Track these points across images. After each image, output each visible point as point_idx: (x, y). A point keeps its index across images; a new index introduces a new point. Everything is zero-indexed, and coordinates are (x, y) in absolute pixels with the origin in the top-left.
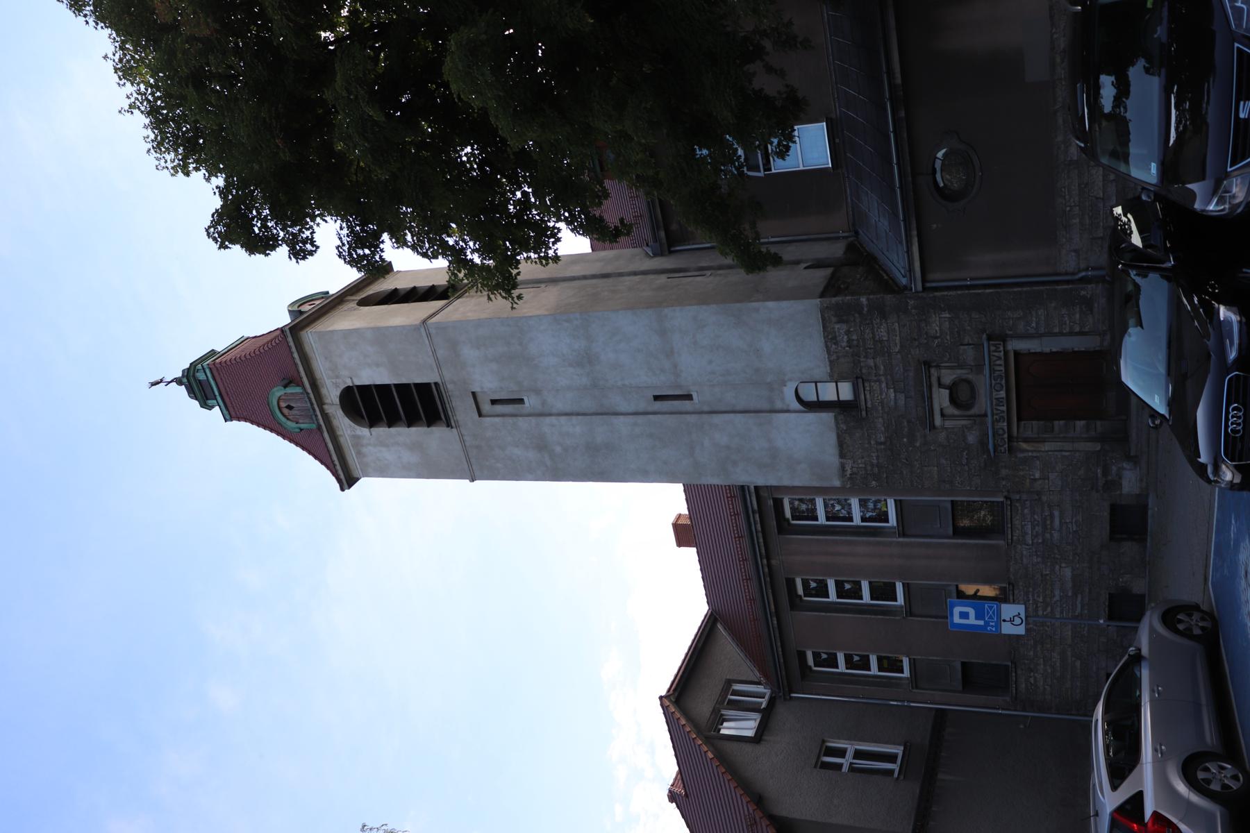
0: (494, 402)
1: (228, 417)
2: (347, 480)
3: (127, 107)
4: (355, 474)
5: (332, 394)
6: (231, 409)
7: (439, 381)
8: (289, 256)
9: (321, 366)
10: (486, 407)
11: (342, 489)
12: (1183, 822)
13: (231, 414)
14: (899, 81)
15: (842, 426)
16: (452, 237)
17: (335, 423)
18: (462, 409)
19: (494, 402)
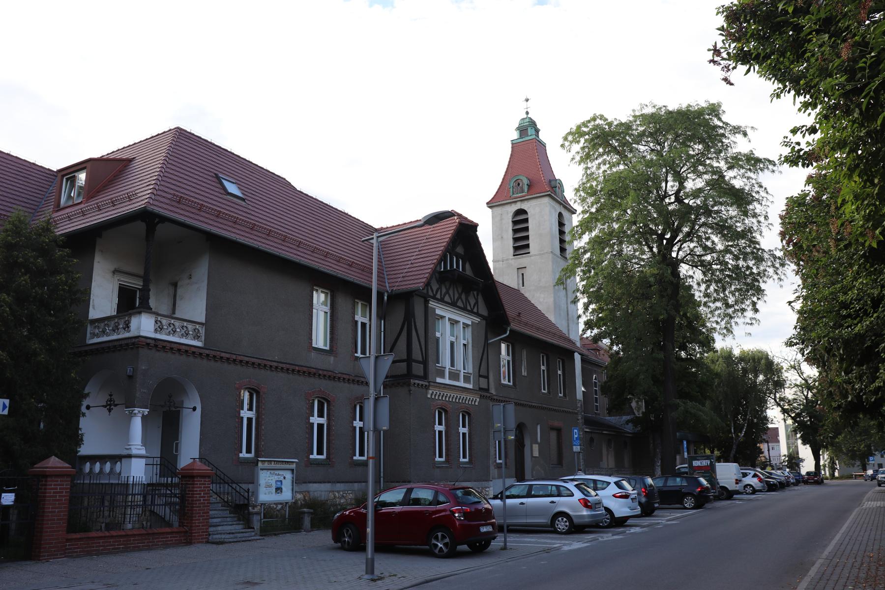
0: (523, 274)
1: (514, 142)
2: (491, 204)
3: (771, 279)
4: (495, 209)
5: (524, 206)
6: (522, 143)
7: (530, 254)
8: (108, 585)
9: (533, 203)
10: (521, 271)
11: (488, 203)
12: (302, 524)
13: (514, 145)
14: (625, 435)
15: (696, 146)
16: (812, 3)
17: (513, 205)
18: (523, 261)
19: (523, 274)
